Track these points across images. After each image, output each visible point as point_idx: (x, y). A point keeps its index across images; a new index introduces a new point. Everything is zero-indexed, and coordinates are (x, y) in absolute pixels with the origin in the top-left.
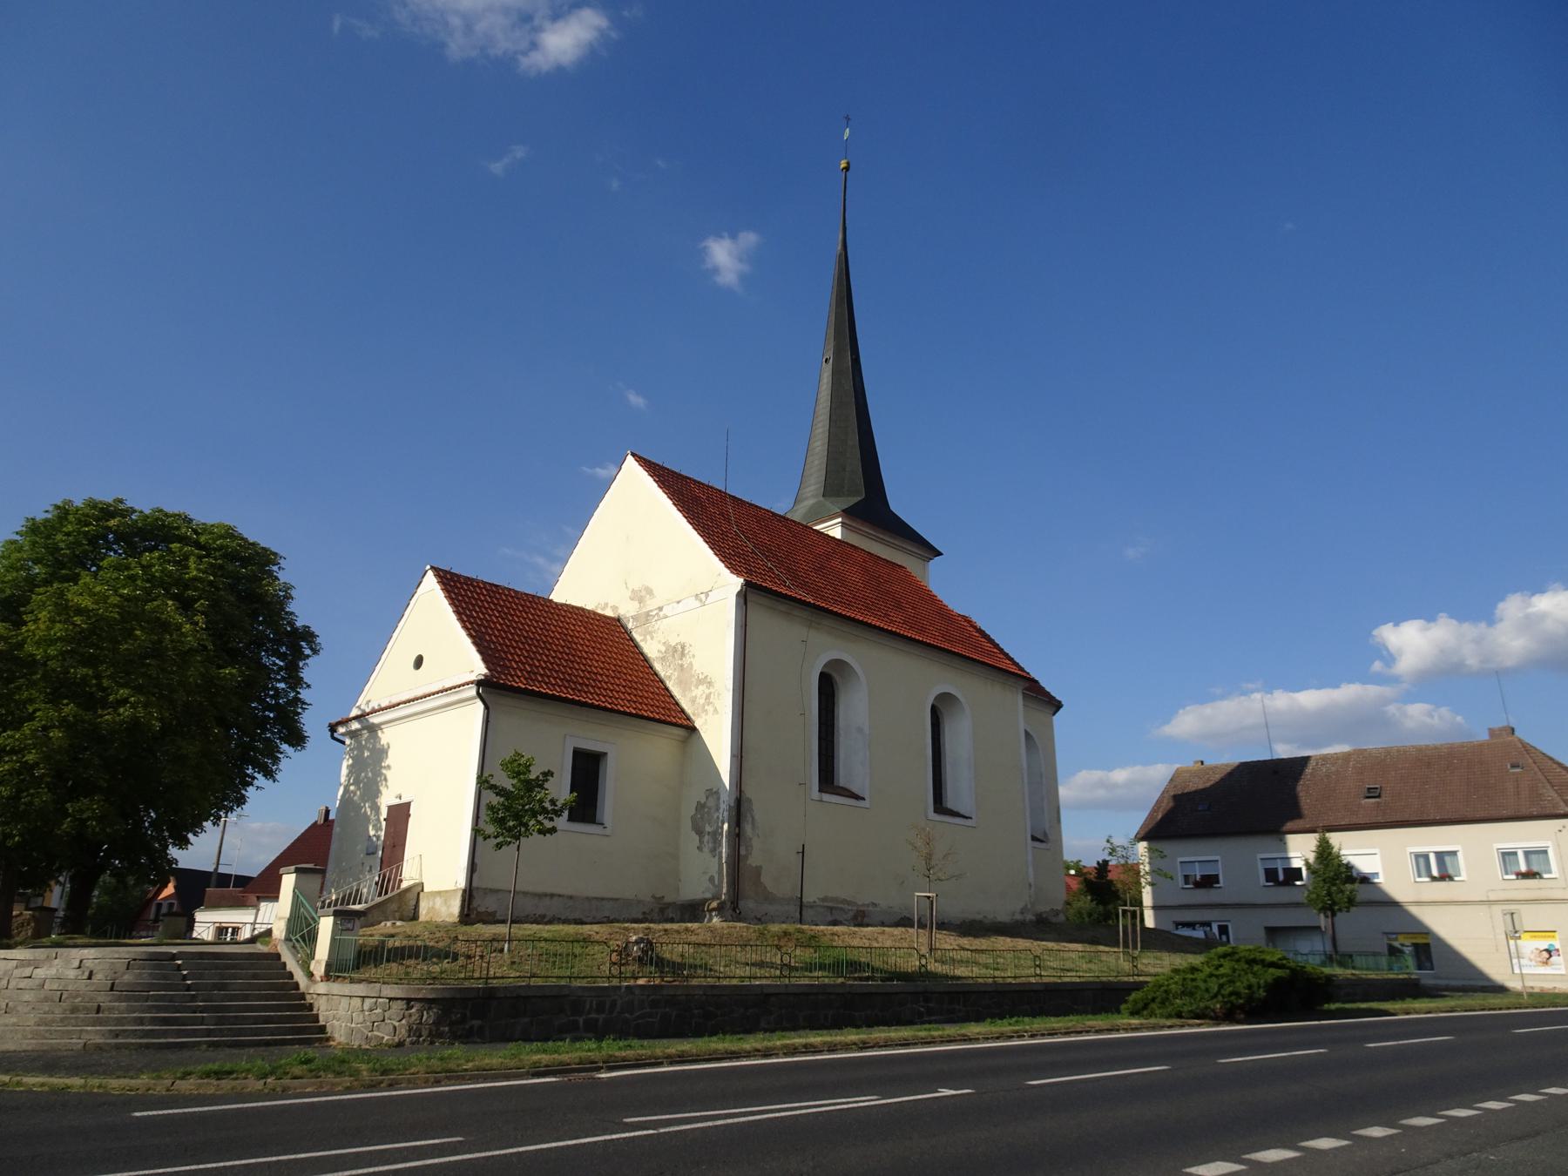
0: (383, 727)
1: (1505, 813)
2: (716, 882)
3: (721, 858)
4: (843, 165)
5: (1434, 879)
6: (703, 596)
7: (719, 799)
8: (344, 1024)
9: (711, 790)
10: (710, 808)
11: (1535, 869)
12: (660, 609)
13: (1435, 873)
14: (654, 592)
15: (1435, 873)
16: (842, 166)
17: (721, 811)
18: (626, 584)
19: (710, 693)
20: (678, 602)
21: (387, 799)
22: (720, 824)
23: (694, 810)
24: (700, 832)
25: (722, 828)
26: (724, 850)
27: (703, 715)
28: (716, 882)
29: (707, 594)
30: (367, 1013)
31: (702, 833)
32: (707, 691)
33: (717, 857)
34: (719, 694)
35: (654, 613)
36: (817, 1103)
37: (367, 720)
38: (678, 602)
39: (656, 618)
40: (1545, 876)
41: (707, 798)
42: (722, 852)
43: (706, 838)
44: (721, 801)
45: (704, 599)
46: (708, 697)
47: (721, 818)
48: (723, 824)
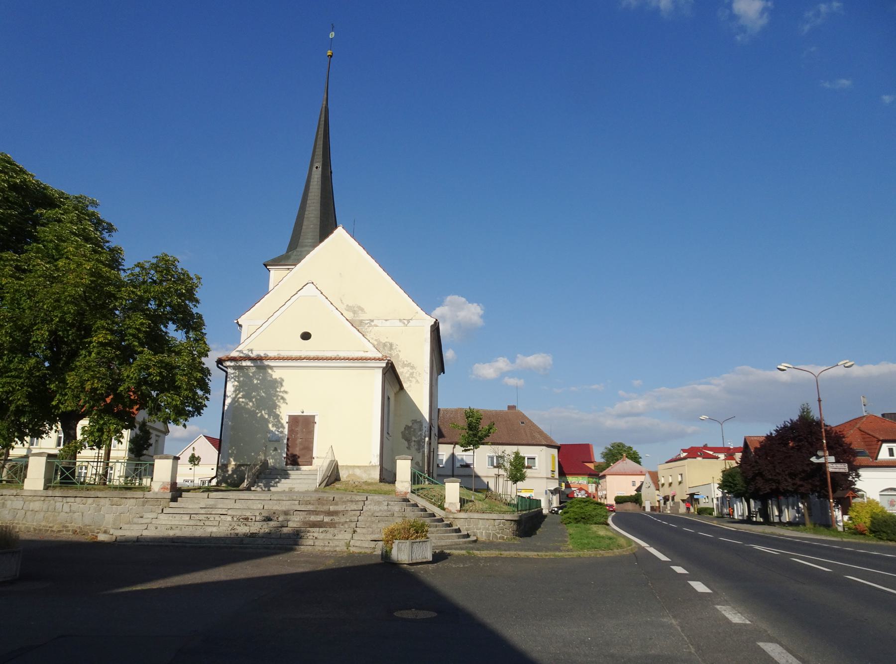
0: (274, 368)
1: (524, 442)
2: (421, 465)
3: (424, 454)
4: (329, 53)
5: (495, 467)
6: (406, 322)
7: (422, 425)
8: (484, 532)
9: (416, 420)
10: (415, 429)
11: (530, 465)
12: (372, 321)
13: (495, 465)
14: (365, 310)
15: (495, 465)
16: (329, 54)
17: (424, 431)
18: (341, 301)
19: (413, 372)
20: (386, 320)
21: (285, 412)
22: (423, 438)
23: (403, 429)
24: (408, 440)
25: (424, 439)
26: (426, 450)
27: (408, 382)
28: (421, 465)
29: (409, 321)
30: (497, 526)
31: (409, 440)
32: (411, 371)
33: (421, 453)
34: (420, 374)
35: (367, 322)
36: (772, 552)
37: (263, 363)
38: (386, 320)
39: (368, 325)
40: (533, 468)
41: (413, 424)
42: (424, 451)
43: (413, 443)
44: (423, 426)
45: (406, 323)
46: (412, 374)
47: (424, 435)
48: (425, 437)
